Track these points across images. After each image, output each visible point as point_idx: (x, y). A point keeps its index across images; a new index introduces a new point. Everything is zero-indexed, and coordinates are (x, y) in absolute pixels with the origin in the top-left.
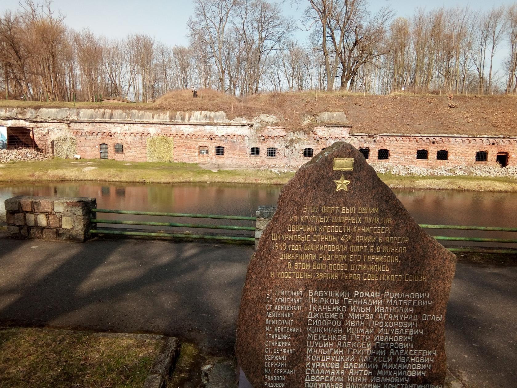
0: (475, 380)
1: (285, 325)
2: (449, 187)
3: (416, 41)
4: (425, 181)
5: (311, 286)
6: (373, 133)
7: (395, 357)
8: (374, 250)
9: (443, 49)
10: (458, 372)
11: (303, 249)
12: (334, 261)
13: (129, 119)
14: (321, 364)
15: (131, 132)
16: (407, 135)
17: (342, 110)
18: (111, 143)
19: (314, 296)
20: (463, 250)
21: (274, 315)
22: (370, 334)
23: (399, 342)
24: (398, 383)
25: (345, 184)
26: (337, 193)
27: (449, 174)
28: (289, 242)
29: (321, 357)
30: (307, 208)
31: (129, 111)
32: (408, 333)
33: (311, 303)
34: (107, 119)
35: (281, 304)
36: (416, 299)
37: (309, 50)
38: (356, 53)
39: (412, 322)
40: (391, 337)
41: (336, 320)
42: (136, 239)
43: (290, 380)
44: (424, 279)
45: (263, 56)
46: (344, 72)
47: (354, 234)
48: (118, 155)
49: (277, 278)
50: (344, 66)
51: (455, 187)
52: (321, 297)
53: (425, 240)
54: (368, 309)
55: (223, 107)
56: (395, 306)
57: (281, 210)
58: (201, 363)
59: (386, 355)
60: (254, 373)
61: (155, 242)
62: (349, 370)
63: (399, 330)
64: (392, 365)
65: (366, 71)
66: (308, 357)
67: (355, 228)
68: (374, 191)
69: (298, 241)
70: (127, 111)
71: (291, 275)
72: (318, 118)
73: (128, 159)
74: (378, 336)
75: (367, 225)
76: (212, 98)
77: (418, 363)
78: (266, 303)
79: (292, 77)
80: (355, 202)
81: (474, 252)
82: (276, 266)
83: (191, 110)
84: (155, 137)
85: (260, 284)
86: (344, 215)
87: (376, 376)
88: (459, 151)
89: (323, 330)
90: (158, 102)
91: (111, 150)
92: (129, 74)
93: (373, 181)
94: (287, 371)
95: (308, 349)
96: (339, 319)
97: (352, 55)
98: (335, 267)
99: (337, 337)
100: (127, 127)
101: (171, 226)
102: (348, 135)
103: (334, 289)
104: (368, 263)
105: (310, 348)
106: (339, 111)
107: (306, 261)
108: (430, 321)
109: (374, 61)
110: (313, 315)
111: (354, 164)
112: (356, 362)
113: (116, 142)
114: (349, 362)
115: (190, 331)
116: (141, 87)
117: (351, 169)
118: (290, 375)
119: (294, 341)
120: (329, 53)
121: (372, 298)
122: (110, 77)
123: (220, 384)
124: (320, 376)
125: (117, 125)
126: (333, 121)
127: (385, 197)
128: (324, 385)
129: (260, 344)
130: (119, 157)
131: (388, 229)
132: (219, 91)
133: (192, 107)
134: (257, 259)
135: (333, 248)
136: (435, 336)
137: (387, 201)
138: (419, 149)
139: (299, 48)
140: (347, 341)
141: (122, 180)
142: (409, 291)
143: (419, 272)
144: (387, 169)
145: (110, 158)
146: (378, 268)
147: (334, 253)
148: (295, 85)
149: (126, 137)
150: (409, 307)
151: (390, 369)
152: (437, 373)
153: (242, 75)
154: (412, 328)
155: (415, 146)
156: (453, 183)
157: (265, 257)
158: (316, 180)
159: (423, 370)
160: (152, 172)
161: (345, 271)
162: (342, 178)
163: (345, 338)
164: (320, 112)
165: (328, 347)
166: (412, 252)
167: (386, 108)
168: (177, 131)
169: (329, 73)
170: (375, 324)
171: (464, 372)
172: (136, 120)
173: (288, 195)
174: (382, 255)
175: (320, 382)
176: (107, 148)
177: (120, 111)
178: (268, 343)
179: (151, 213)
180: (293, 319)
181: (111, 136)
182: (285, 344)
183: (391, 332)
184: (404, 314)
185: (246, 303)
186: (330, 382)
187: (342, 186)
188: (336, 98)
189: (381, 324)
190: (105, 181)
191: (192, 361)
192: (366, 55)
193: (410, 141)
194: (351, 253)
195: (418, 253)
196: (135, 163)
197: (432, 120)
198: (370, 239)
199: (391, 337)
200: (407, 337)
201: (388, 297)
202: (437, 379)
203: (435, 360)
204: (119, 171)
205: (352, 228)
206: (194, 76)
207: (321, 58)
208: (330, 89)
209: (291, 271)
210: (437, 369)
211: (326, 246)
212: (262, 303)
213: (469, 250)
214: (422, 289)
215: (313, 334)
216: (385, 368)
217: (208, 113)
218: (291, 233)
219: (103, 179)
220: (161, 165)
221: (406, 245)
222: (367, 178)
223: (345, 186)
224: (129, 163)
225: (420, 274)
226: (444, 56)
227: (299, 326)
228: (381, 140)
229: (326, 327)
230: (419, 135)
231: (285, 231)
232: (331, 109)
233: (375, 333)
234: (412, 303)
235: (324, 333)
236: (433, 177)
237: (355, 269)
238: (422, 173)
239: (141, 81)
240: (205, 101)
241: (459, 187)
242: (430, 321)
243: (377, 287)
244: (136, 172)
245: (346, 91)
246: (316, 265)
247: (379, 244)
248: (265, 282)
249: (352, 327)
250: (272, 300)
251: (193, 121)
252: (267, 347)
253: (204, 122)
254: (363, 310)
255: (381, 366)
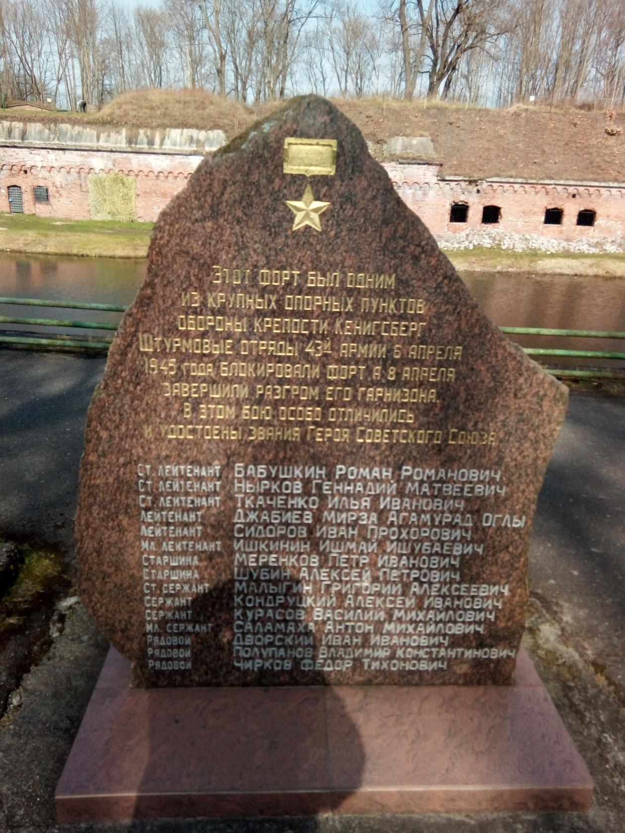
0: (584, 620)
1: (184, 538)
2: (591, 272)
3: (564, 8)
4: (553, 261)
5: (241, 457)
6: (476, 176)
7: (420, 599)
8: (383, 376)
9: (610, 25)
10: (557, 604)
11: (218, 374)
12: (290, 400)
13: (57, 142)
14: (266, 613)
15: (61, 164)
16: (533, 181)
17: (427, 134)
18: (26, 183)
19: (246, 478)
20: (598, 374)
21: (158, 517)
22: (368, 554)
23: (430, 569)
24: (428, 647)
25: (316, 210)
26: (295, 234)
27: (594, 250)
28: (183, 357)
29: (266, 599)
30: (220, 273)
31: (55, 125)
32: (451, 551)
33: (240, 492)
34: (17, 141)
35: (174, 494)
36: (471, 482)
37: (375, 19)
38: (457, 29)
39: (461, 528)
40: (415, 559)
41: (296, 525)
42: (16, 349)
43: (202, 644)
44: (491, 439)
45: (294, 28)
46: (435, 65)
47: (335, 339)
48: (40, 206)
49: (160, 438)
50: (435, 53)
51: (601, 272)
52: (263, 479)
53: (500, 352)
54: (366, 503)
55: (221, 122)
56: (425, 495)
57: (156, 275)
58: (59, 593)
59: (403, 594)
60: (123, 631)
61: (49, 355)
62: (324, 622)
63: (432, 546)
64: (414, 613)
65: (473, 66)
66: (238, 600)
67: (338, 325)
68: (387, 231)
69: (204, 355)
70: (52, 125)
71: (193, 431)
72: (385, 147)
73: (60, 214)
74: (386, 557)
75: (367, 317)
76: (202, 106)
77: (469, 610)
78: (138, 493)
79: (346, 72)
80: (339, 258)
81: (616, 379)
82: (155, 411)
83: (164, 126)
84: (103, 175)
85: (121, 451)
86: (312, 291)
87: (382, 634)
88: (613, 211)
89: (268, 546)
90: (106, 110)
91: (27, 197)
92: (57, 58)
93: (384, 203)
94: (194, 627)
95: (237, 584)
96: (302, 524)
97: (450, 34)
98: (293, 413)
99: (298, 560)
100: (52, 155)
101: (75, 326)
102: (435, 180)
103: (290, 461)
104: (367, 405)
105: (241, 582)
106: (422, 136)
107: (225, 401)
108: (499, 528)
109: (487, 45)
110: (246, 515)
111: (338, 157)
112: (340, 607)
113: (36, 184)
114: (325, 608)
115: (57, 527)
116: (79, 82)
117: (329, 170)
118: (201, 635)
119: (206, 568)
120: (410, 27)
121: (375, 480)
122: (21, 60)
123: (85, 638)
124: (264, 634)
125: (36, 151)
126: (411, 153)
127: (412, 247)
128: (273, 652)
129: (132, 576)
130: (41, 210)
131: (416, 327)
132: (216, 93)
133: (166, 121)
134: (109, 396)
135: (287, 371)
136: (507, 558)
137: (416, 258)
138: (550, 207)
139: (359, 17)
140: (321, 567)
141: (48, 250)
142: (456, 466)
143: (480, 426)
144: (494, 239)
145: (27, 212)
146: (381, 418)
147: (289, 382)
148: (351, 87)
149: (52, 173)
150: (455, 498)
151: (411, 622)
152: (507, 628)
153: (257, 65)
154: (460, 541)
155: (546, 202)
156: (597, 265)
157: (127, 391)
158: (242, 198)
159: (479, 623)
160: (100, 238)
161: (315, 423)
162: (308, 195)
163: (315, 560)
164: (390, 136)
165: (280, 580)
166: (469, 381)
167: (502, 132)
168: (140, 165)
169: (410, 70)
170: (383, 532)
171: (567, 605)
172: (69, 143)
173: (171, 236)
174: (399, 387)
175: (265, 647)
176: (21, 194)
177: (39, 126)
178: (150, 574)
179: (36, 301)
180: (202, 524)
181: (26, 172)
182: (188, 574)
183: (413, 549)
184: (443, 512)
185: (91, 494)
186: (285, 647)
187: (307, 216)
188: (419, 111)
189: (394, 533)
190: (20, 252)
191: (39, 589)
192: (474, 34)
193: (537, 193)
194: (330, 383)
195: (482, 382)
196: (70, 221)
197: (575, 157)
198: (375, 350)
199: (415, 559)
200: (447, 560)
201: (410, 478)
202: (505, 638)
203: (504, 603)
204: (43, 235)
205: (332, 324)
206: (172, 65)
207: (397, 35)
208: (409, 96)
209: (191, 423)
210: (508, 620)
211: (270, 368)
212: (128, 492)
213: (609, 374)
214: (484, 461)
215: (248, 554)
216: (400, 620)
217: (194, 132)
218: (186, 335)
219: (16, 248)
220: (116, 226)
221: (455, 364)
222: (369, 195)
223: (315, 217)
224: (60, 220)
225: (483, 430)
226: (609, 39)
227: (215, 539)
228: (489, 190)
229: (275, 540)
230: (552, 182)
231: (171, 330)
232: (408, 131)
233: (380, 551)
234: (462, 490)
235: (270, 553)
236: (567, 254)
237: (338, 417)
238: (550, 248)
239: (78, 71)
240: (190, 111)
241: (607, 272)
242: (499, 528)
243: (387, 457)
244: (72, 237)
245: (437, 100)
246: (250, 410)
247: (395, 363)
248: (132, 447)
249: (331, 540)
250: (152, 485)
251: (168, 146)
252: (147, 581)
253: (187, 148)
254: (355, 505)
255: (391, 616)
